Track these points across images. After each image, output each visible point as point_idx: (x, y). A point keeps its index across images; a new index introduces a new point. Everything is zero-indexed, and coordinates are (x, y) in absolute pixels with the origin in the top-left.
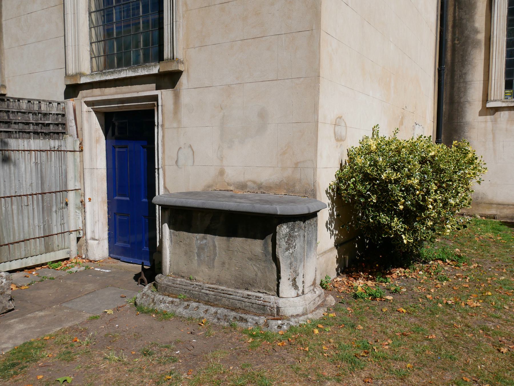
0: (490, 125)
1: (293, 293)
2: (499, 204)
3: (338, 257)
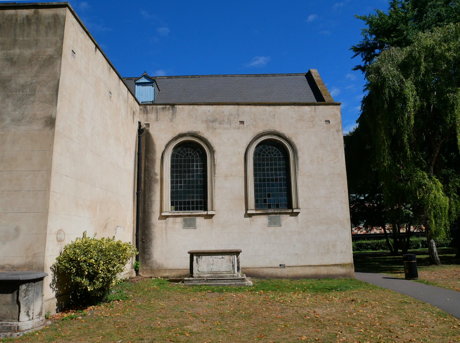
0: (164, 225)
1: (27, 318)
2: (170, 270)
3: (57, 303)
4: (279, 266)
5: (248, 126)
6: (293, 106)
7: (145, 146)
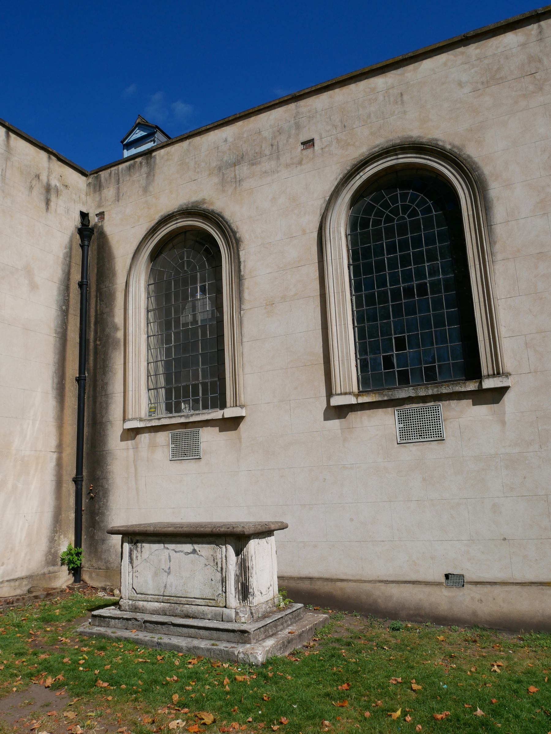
0: (131, 452)
4: (443, 580)
5: (327, 149)
6: (462, 49)
7: (97, 264)
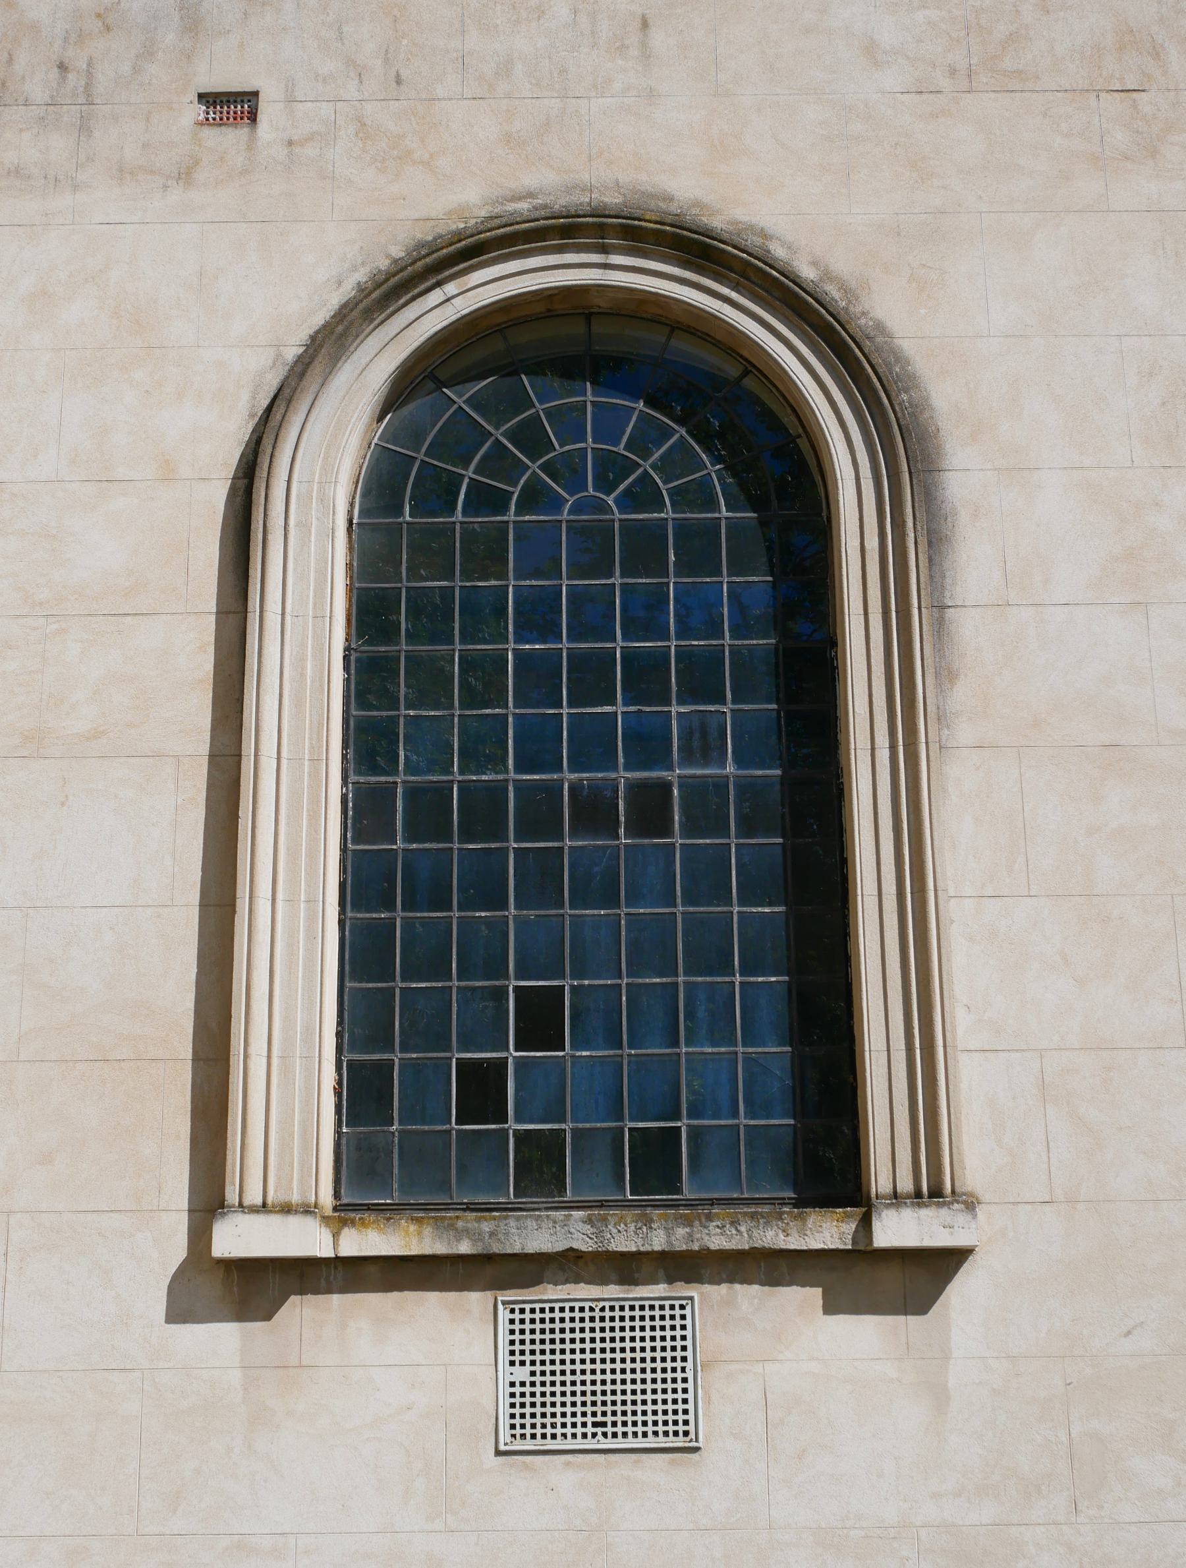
5: (310, 151)
